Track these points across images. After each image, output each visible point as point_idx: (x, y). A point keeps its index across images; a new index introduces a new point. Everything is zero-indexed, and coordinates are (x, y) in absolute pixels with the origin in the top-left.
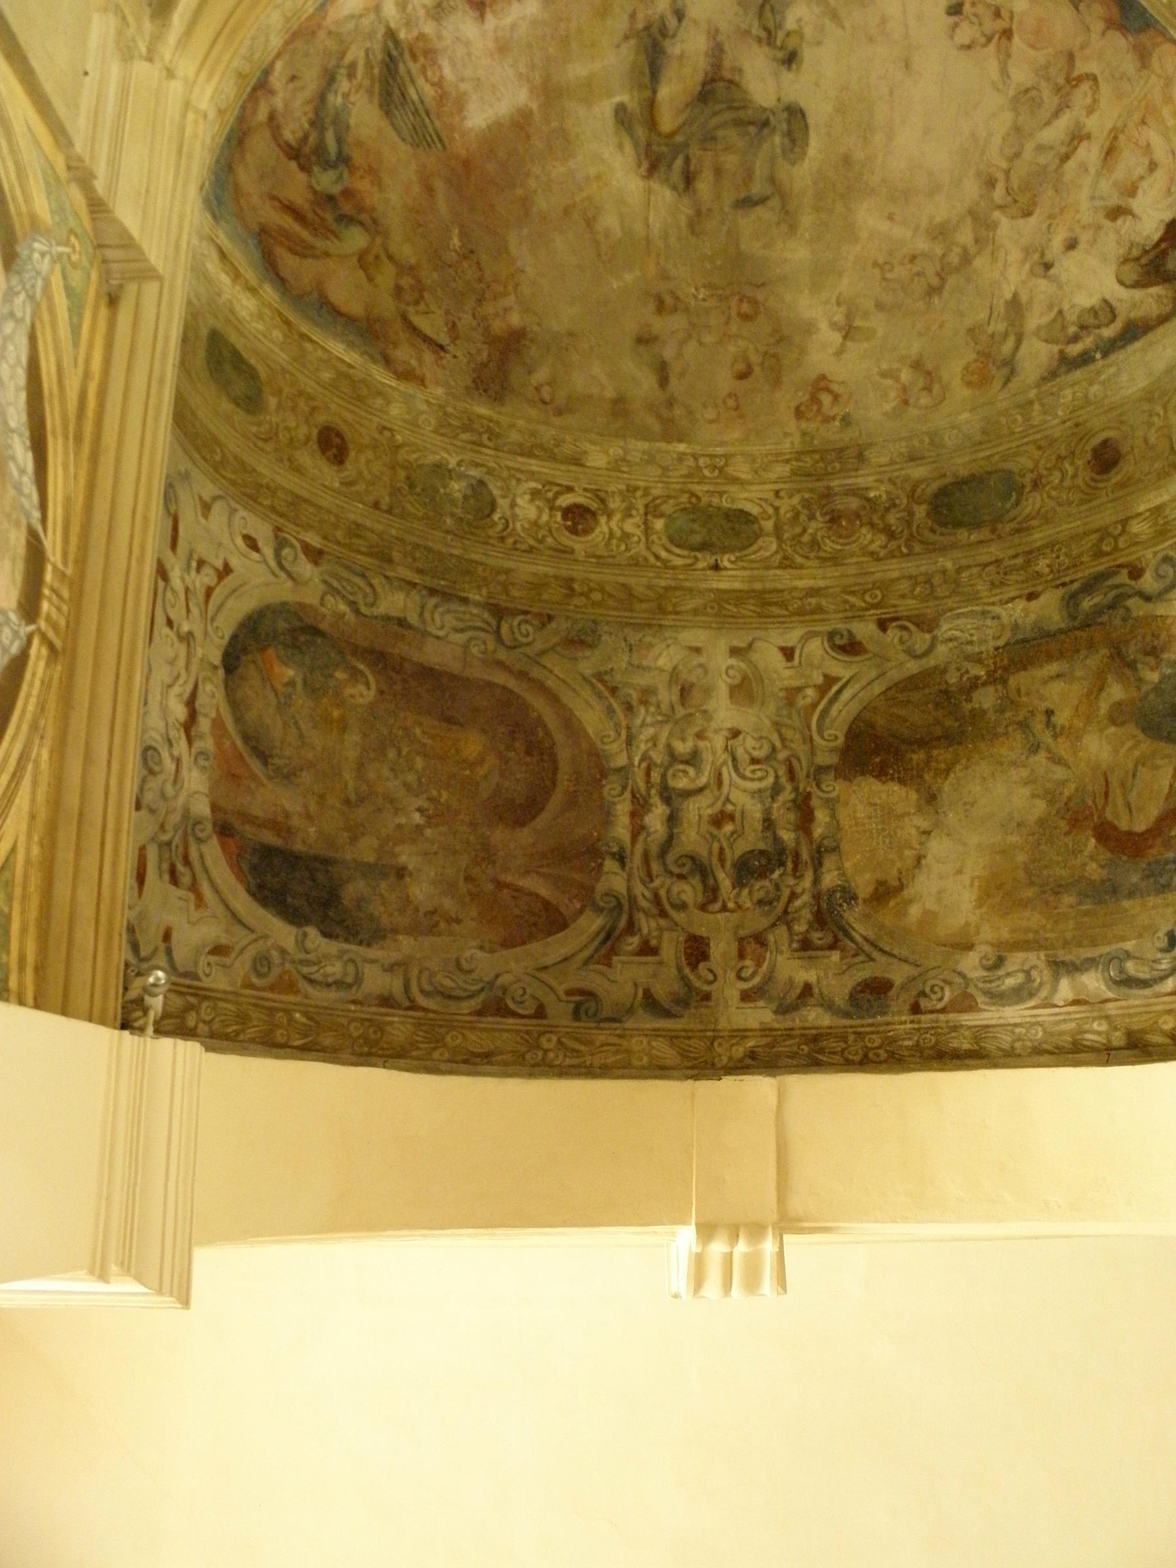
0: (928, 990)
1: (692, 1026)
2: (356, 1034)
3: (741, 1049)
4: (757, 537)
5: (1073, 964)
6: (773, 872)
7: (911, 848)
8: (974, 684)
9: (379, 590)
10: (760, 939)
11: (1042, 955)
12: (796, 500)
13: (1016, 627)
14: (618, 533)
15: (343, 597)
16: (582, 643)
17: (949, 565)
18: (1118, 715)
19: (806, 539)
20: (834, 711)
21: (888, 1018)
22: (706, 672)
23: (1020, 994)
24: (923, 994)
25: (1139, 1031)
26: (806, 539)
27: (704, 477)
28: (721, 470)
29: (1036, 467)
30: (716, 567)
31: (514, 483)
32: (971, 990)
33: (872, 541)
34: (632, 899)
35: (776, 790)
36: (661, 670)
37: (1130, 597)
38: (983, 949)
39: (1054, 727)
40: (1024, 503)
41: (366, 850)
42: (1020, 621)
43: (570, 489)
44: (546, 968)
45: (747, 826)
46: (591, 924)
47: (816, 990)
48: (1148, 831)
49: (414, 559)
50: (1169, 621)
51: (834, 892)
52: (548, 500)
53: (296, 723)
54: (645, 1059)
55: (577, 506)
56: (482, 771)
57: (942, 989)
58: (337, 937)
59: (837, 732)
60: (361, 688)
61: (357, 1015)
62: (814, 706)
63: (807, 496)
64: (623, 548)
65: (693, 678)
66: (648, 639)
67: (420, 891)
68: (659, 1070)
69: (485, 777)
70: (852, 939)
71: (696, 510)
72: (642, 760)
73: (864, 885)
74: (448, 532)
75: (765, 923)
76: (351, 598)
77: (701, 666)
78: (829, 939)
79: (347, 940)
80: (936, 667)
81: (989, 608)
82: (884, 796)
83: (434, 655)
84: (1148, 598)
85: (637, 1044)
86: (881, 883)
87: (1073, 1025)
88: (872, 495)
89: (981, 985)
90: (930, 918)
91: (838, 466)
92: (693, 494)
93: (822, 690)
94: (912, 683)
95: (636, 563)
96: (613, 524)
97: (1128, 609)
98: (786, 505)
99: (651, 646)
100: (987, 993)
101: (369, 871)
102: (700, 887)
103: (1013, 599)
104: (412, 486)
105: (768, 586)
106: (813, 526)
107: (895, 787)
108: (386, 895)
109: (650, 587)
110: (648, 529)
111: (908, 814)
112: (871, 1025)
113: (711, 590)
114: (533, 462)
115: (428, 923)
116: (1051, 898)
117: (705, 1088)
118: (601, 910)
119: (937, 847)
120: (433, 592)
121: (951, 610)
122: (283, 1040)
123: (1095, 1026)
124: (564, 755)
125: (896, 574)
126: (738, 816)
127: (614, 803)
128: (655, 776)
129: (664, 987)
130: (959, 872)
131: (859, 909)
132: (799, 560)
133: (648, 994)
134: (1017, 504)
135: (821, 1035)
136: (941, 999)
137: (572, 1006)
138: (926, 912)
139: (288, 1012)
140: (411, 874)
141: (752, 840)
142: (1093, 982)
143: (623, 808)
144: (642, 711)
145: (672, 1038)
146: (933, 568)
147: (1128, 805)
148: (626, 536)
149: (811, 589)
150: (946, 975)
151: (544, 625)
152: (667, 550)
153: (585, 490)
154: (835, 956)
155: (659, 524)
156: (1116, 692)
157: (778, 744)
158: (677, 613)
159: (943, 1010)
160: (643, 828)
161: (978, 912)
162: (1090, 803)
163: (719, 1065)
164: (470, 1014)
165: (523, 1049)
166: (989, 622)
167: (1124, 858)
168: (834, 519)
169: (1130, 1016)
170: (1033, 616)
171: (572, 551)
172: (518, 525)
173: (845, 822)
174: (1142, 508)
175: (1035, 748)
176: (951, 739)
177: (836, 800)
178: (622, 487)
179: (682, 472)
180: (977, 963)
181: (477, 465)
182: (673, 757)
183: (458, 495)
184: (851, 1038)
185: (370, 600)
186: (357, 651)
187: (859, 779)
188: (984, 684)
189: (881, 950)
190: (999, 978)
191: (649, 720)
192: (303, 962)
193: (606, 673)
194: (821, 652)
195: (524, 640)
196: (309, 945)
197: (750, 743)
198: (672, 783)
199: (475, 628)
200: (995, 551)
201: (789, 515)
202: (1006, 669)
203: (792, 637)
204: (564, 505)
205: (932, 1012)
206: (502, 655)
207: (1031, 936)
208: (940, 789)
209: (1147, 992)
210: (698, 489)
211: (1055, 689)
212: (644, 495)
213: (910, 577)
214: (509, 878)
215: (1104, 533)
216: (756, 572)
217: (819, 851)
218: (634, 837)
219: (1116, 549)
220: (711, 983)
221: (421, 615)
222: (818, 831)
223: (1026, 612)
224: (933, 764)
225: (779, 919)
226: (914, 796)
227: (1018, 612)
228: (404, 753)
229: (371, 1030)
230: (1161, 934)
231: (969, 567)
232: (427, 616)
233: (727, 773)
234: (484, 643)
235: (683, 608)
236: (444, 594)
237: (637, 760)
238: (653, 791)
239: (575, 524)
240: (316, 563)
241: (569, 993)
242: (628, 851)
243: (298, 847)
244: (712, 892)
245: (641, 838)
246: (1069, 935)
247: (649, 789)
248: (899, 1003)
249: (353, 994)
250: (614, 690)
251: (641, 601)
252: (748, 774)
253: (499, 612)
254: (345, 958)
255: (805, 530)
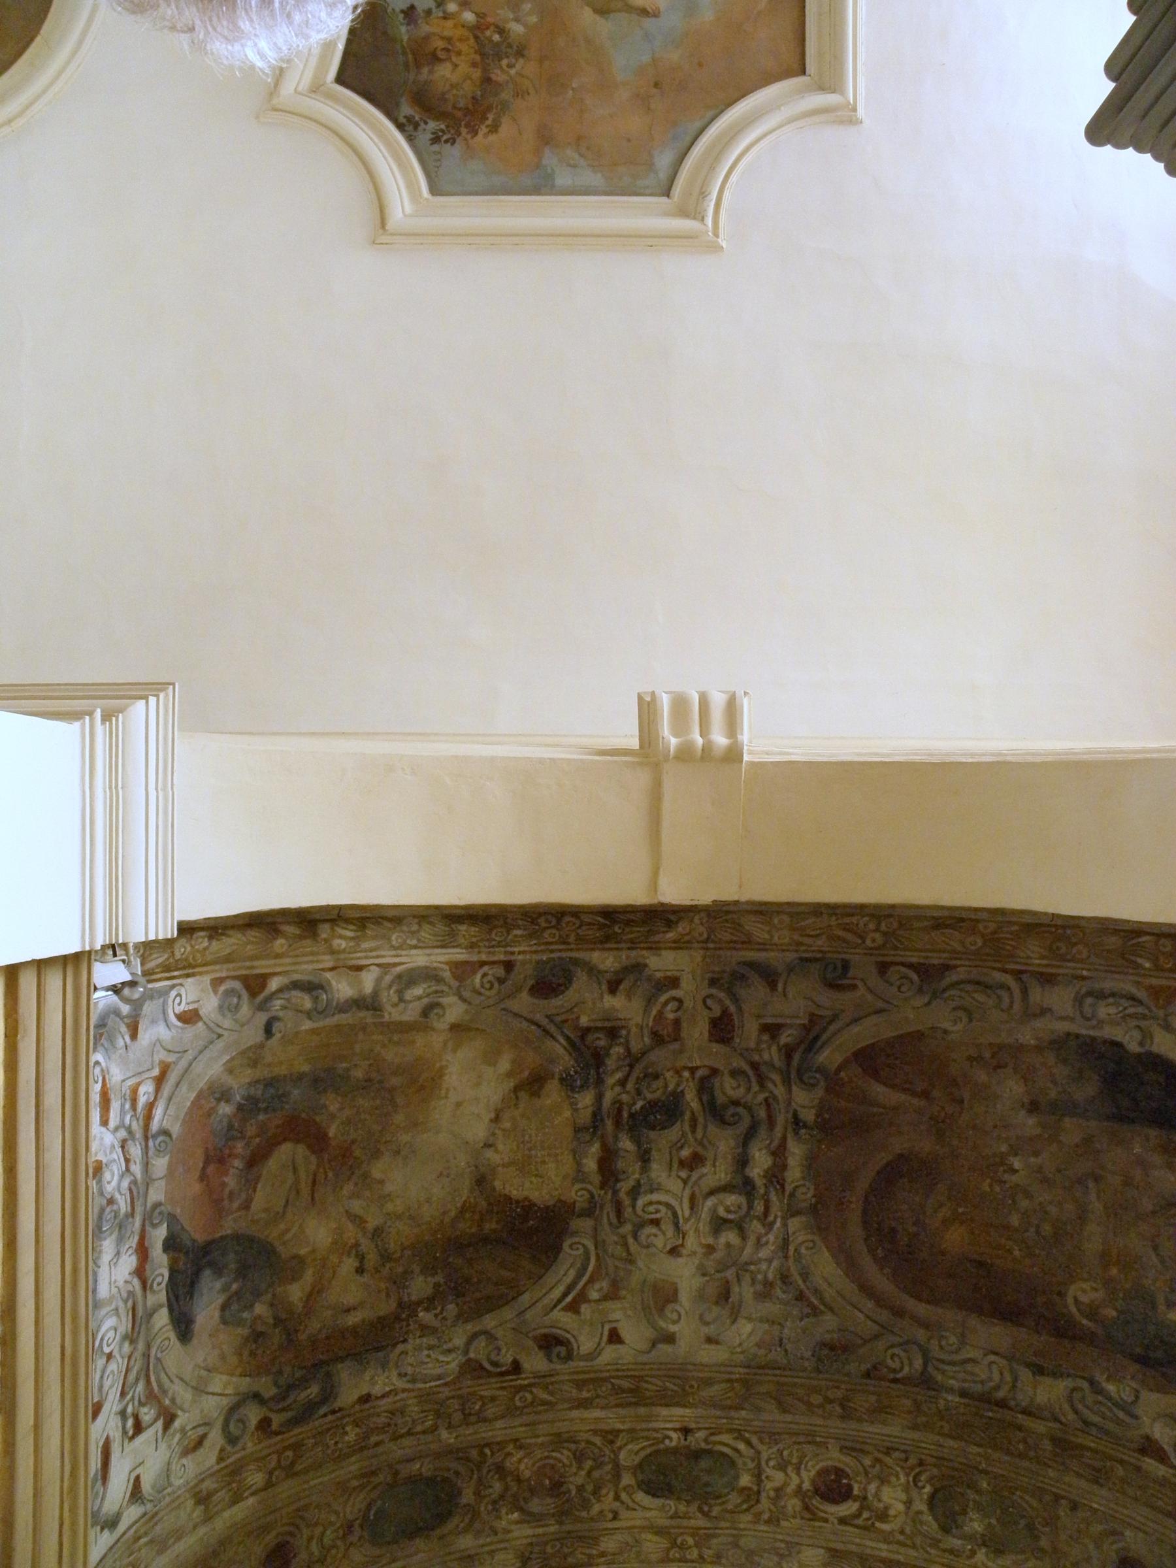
0: (496, 985)
1: (729, 953)
2: (1080, 947)
3: (680, 929)
4: (640, 1466)
5: (359, 1007)
6: (642, 1108)
7: (504, 1130)
8: (430, 1302)
9: (1066, 1406)
10: (658, 1039)
11: (387, 1018)
12: (596, 1508)
13: (384, 1366)
14: (790, 1469)
15: (1110, 1399)
16: (832, 1348)
17: (444, 1434)
18: (293, 1268)
19: (589, 1464)
20: (572, 1273)
21: (535, 957)
22: (701, 1316)
23: (409, 979)
24: (501, 981)
25: (305, 938)
26: (589, 1464)
27: (693, 1535)
28: (674, 1544)
29: (347, 1550)
30: (686, 1431)
31: (908, 1530)
32: (455, 984)
33: (520, 1461)
34: (787, 1082)
35: (635, 1192)
36: (749, 1319)
37: (272, 1398)
38: (442, 1025)
39: (357, 1256)
40: (363, 1506)
41: (1072, 1130)
42: (380, 1371)
43: (843, 1521)
44: (878, 1012)
45: (667, 1156)
46: (829, 1056)
47: (604, 987)
48: (280, 1143)
49: (1025, 1441)
50: (240, 1370)
51: (582, 1086)
52: (869, 1508)
53: (1163, 1262)
54: (776, 921)
55: (835, 1502)
56: (944, 1212)
57: (482, 986)
58: (1105, 1042)
59: (570, 1253)
60: (1085, 1299)
61: (1079, 965)
62: (591, 1281)
63: (584, 1514)
64: (785, 1453)
65: (716, 1310)
66: (762, 1352)
67: (1012, 1088)
68: (763, 911)
69: (941, 1205)
70: (568, 1038)
71: (703, 1497)
72: (773, 1223)
73: (553, 1093)
74: (986, 1472)
75: (653, 1056)
76: (1100, 1398)
77: (707, 1324)
78: (590, 1038)
79: (1093, 1039)
80: (466, 1321)
81: (410, 1386)
82: (527, 1184)
83: (999, 1334)
84: (256, 1396)
85: (783, 937)
86: (536, 1094)
87: (365, 945)
88: (516, 1515)
89: (445, 989)
90: (491, 1058)
91: (549, 1550)
92: (706, 1515)
93: (582, 1298)
94: (492, 1304)
95: (773, 1437)
96: (795, 1480)
97: (276, 1384)
98: (608, 1502)
99: (758, 1345)
100: (439, 980)
101: (1061, 1108)
102: (717, 1093)
103: (383, 1396)
104: (1030, 1527)
105: (631, 1411)
106: (579, 1480)
107: (515, 1194)
108: (1049, 1085)
109: (759, 1409)
110: (758, 1476)
111: (503, 1166)
112: (552, 951)
113: (691, 1406)
114: (884, 1554)
115: (1002, 1057)
116: (374, 1075)
117: (729, 893)
118: (818, 1070)
119: (478, 1131)
120: (1002, 1404)
121: (446, 1384)
122: (1163, 941)
123: (343, 944)
124: (855, 1229)
125: (499, 1424)
126: (675, 1166)
127: (803, 1178)
128: (759, 1207)
129: (755, 993)
130: (459, 1105)
131: (558, 1069)
132: (597, 1440)
133: (773, 985)
134: (369, 1506)
135: (602, 942)
136: (485, 975)
137: (850, 974)
138: (494, 1064)
139: (1158, 967)
140: (1023, 1106)
141: (663, 1140)
142: (342, 988)
143: (794, 1173)
144: (770, 1276)
145: (749, 942)
146: (461, 1430)
147: (295, 1170)
148: (782, 1467)
149: (586, 1408)
150: (477, 1000)
151: (875, 1367)
152: (736, 1450)
153: (826, 1521)
154: (584, 1021)
155: (745, 1480)
156: (296, 1293)
157: (631, 1240)
158: (729, 1381)
159: (483, 964)
160: (774, 1154)
161: (444, 1063)
162: (330, 1174)
163: (703, 914)
164: (956, 967)
165: (901, 932)
166: (410, 1370)
167: (303, 1115)
168: (557, 1488)
169: (312, 954)
170: (367, 1376)
171: (842, 1448)
172: (903, 1479)
173: (567, 1159)
174: (251, 1500)
175: (378, 1233)
176: (458, 1245)
177: (576, 1180)
178: (784, 1523)
179: (715, 1541)
180: (448, 1013)
181: (951, 1551)
182: (740, 1227)
183: (973, 1515)
184: (572, 939)
185: (1077, 1396)
186: (1089, 1338)
187: (551, 1203)
188: (419, 1303)
189: (539, 1026)
190: (428, 995)
191: (764, 1266)
192: (1144, 1017)
193: (808, 1316)
194: (582, 1338)
195: (896, 1351)
196: (1137, 1035)
197: (659, 1242)
198: (742, 1200)
199: (953, 1363)
200: (397, 1451)
201: (604, 1491)
202: (398, 1318)
203: (609, 1354)
204: (850, 1502)
205: (494, 963)
206: (921, 1335)
207: (396, 1038)
208: (471, 1191)
209: (296, 977)
210: (701, 1522)
211: (352, 1295)
212: (760, 1513)
213: (485, 1420)
214: (915, 1101)
215: (290, 1471)
216: (644, 1426)
217: (595, 1127)
218: (783, 1145)
219: (280, 1453)
220: (710, 996)
221: (1015, 1379)
222: (595, 1148)
223: (373, 1382)
224: (477, 1217)
225: (637, 1060)
226: (498, 1184)
227: (378, 1381)
228: (1032, 1230)
229: (1063, 950)
230: (278, 1035)
231: (424, 1432)
232: (1008, 1377)
233: (684, 1210)
234: (941, 1347)
235: (723, 1385)
236: (989, 1402)
237: (778, 1224)
238: (762, 1191)
239: (838, 1481)
240: (1148, 1438)
241: (854, 987)
242: (790, 1129)
243: (1153, 1133)
244: (704, 1087)
245: (776, 1143)
246: (361, 1036)
247: (767, 1193)
248: (524, 973)
249: (1084, 987)
250: (800, 1297)
251: (768, 1393)
252: (663, 1209)
253: (925, 1381)
254: (1094, 1022)
255: (589, 1473)
